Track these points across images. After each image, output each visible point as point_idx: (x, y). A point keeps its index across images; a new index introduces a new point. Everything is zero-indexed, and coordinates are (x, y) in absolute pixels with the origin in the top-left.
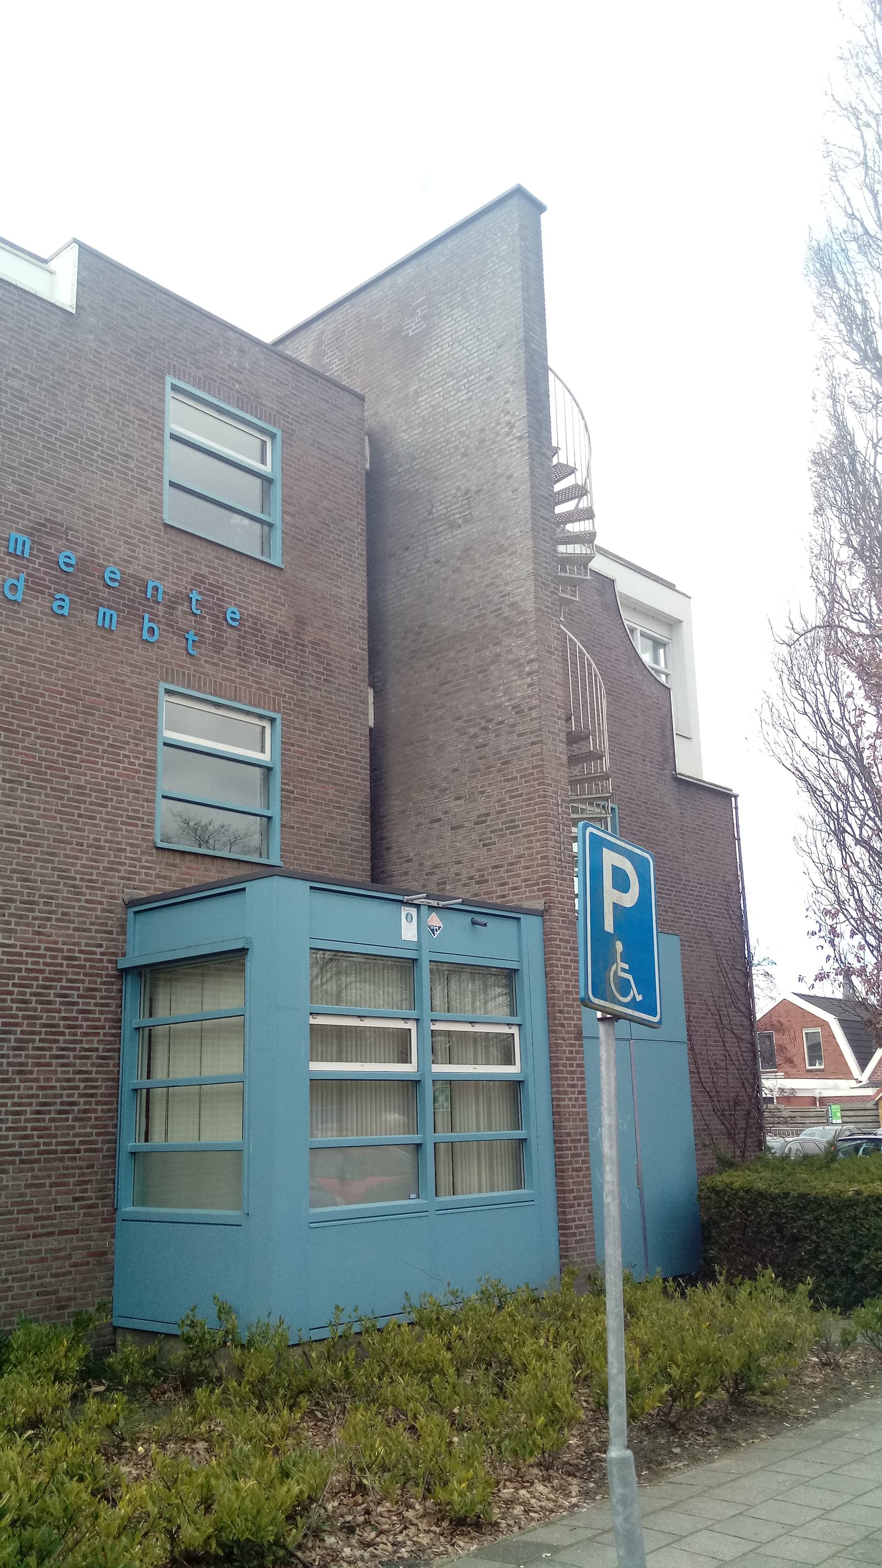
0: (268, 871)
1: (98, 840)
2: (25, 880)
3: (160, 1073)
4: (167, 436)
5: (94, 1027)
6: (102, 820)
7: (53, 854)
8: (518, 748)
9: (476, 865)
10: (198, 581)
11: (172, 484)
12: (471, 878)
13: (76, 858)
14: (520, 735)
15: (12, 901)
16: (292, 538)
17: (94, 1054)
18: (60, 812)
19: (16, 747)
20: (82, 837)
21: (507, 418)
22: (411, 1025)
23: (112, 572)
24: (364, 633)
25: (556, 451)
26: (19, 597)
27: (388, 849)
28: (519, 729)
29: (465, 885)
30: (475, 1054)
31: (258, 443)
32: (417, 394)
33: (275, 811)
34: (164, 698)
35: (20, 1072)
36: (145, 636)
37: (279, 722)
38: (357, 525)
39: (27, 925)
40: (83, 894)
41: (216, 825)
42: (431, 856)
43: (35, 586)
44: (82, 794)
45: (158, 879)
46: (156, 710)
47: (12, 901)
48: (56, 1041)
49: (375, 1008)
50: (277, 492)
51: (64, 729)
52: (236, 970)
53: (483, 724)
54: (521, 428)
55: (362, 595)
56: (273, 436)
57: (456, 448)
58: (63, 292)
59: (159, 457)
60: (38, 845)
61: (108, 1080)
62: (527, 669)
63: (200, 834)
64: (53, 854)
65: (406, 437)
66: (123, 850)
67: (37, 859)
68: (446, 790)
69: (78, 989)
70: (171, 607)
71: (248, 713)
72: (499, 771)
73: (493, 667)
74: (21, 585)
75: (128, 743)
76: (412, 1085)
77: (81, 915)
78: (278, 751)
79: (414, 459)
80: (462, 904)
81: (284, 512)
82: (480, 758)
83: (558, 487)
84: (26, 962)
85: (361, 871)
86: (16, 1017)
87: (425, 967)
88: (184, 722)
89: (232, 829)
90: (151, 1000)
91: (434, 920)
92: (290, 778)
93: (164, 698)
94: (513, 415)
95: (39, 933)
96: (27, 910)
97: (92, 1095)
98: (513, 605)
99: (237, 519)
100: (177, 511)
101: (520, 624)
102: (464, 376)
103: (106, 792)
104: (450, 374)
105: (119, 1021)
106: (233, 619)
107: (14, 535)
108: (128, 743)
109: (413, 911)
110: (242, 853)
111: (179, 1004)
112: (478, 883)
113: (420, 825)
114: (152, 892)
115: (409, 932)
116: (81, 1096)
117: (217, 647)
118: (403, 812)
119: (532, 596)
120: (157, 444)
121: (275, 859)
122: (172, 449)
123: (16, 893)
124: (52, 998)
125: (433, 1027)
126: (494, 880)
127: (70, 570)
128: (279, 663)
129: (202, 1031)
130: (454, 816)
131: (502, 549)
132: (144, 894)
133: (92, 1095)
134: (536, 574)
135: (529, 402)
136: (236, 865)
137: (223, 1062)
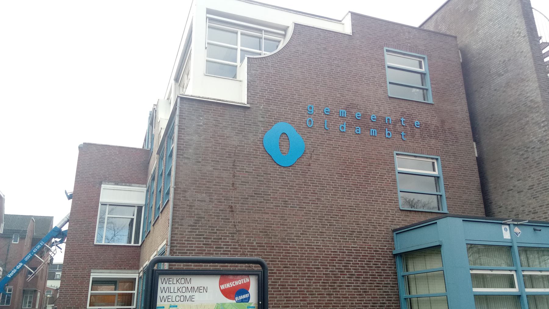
0: (445, 215)
1: (380, 209)
2: (358, 224)
3: (413, 292)
4: (386, 67)
5: (387, 276)
6: (380, 201)
7: (366, 215)
8: (543, 157)
9: (532, 206)
10: (403, 114)
11: (390, 83)
12: (530, 212)
13: (373, 215)
14: (543, 152)
15: (354, 232)
16: (436, 93)
17: (389, 285)
18: (366, 200)
19: (349, 179)
20: (374, 208)
21: (517, 30)
22: (513, 273)
23: (373, 116)
24: (469, 122)
25: (541, 38)
26: (344, 130)
27: (491, 203)
28: (542, 149)
29: (528, 215)
30: (544, 284)
31: (417, 63)
32: (477, 31)
33: (443, 192)
34: (396, 157)
35: (365, 292)
36: (387, 136)
37: (439, 160)
38: (460, 82)
39: (360, 240)
40: (377, 228)
41: (416, 200)
42: (510, 204)
43: (349, 126)
44: (372, 193)
45: (402, 221)
46: (394, 161)
47: (354, 232)
48: (375, 281)
49: (498, 267)
50: (428, 78)
51: (364, 172)
52: (437, 253)
53: (526, 149)
54: (524, 32)
55: (466, 108)
56: (424, 58)
57: (497, 46)
58: (347, 28)
59: (385, 75)
60: (360, 212)
61: (395, 295)
62: (542, 125)
63: (410, 203)
64: (366, 215)
65: (475, 46)
66: (389, 212)
67: (361, 217)
68: (513, 177)
69: (380, 262)
70: (395, 125)
71: (427, 158)
72: (536, 167)
73: (526, 126)
74: (345, 126)
75: (385, 174)
76: (518, 298)
77: (378, 236)
78: (441, 170)
79: (480, 54)
80: (528, 222)
81: (431, 84)
82: (527, 163)
83: (544, 52)
84: (361, 253)
85: (481, 211)
86: (361, 272)
87: (516, 250)
88: (404, 164)
89: (423, 201)
90: (406, 266)
91: (517, 230)
92: (447, 180)
93: (396, 157)
94: (520, 29)
95: (365, 243)
96: (360, 235)
97: (390, 300)
98: (531, 101)
99: (414, 90)
100: (392, 91)
101: (536, 107)
102: (496, 19)
103: (380, 192)
104: (490, 20)
105: (396, 273)
106: (417, 125)
107: (341, 110)
108: (385, 174)
109: (507, 227)
110: (428, 209)
111: (418, 267)
112: (534, 213)
113: (503, 192)
114: (401, 226)
115: (507, 235)
116: (386, 300)
117: (413, 137)
118: (495, 188)
119: (540, 96)
120: (383, 71)
121: (445, 211)
122: (389, 71)
123: (356, 229)
124: (372, 265)
125: (523, 273)
126: (541, 212)
127: (359, 118)
128: (436, 138)
129: (428, 276)
130: (518, 187)
131: (523, 80)
132: (398, 227)
133: (390, 300)
134: (540, 87)
135: (526, 22)
136: (430, 214)
137: (438, 288)
